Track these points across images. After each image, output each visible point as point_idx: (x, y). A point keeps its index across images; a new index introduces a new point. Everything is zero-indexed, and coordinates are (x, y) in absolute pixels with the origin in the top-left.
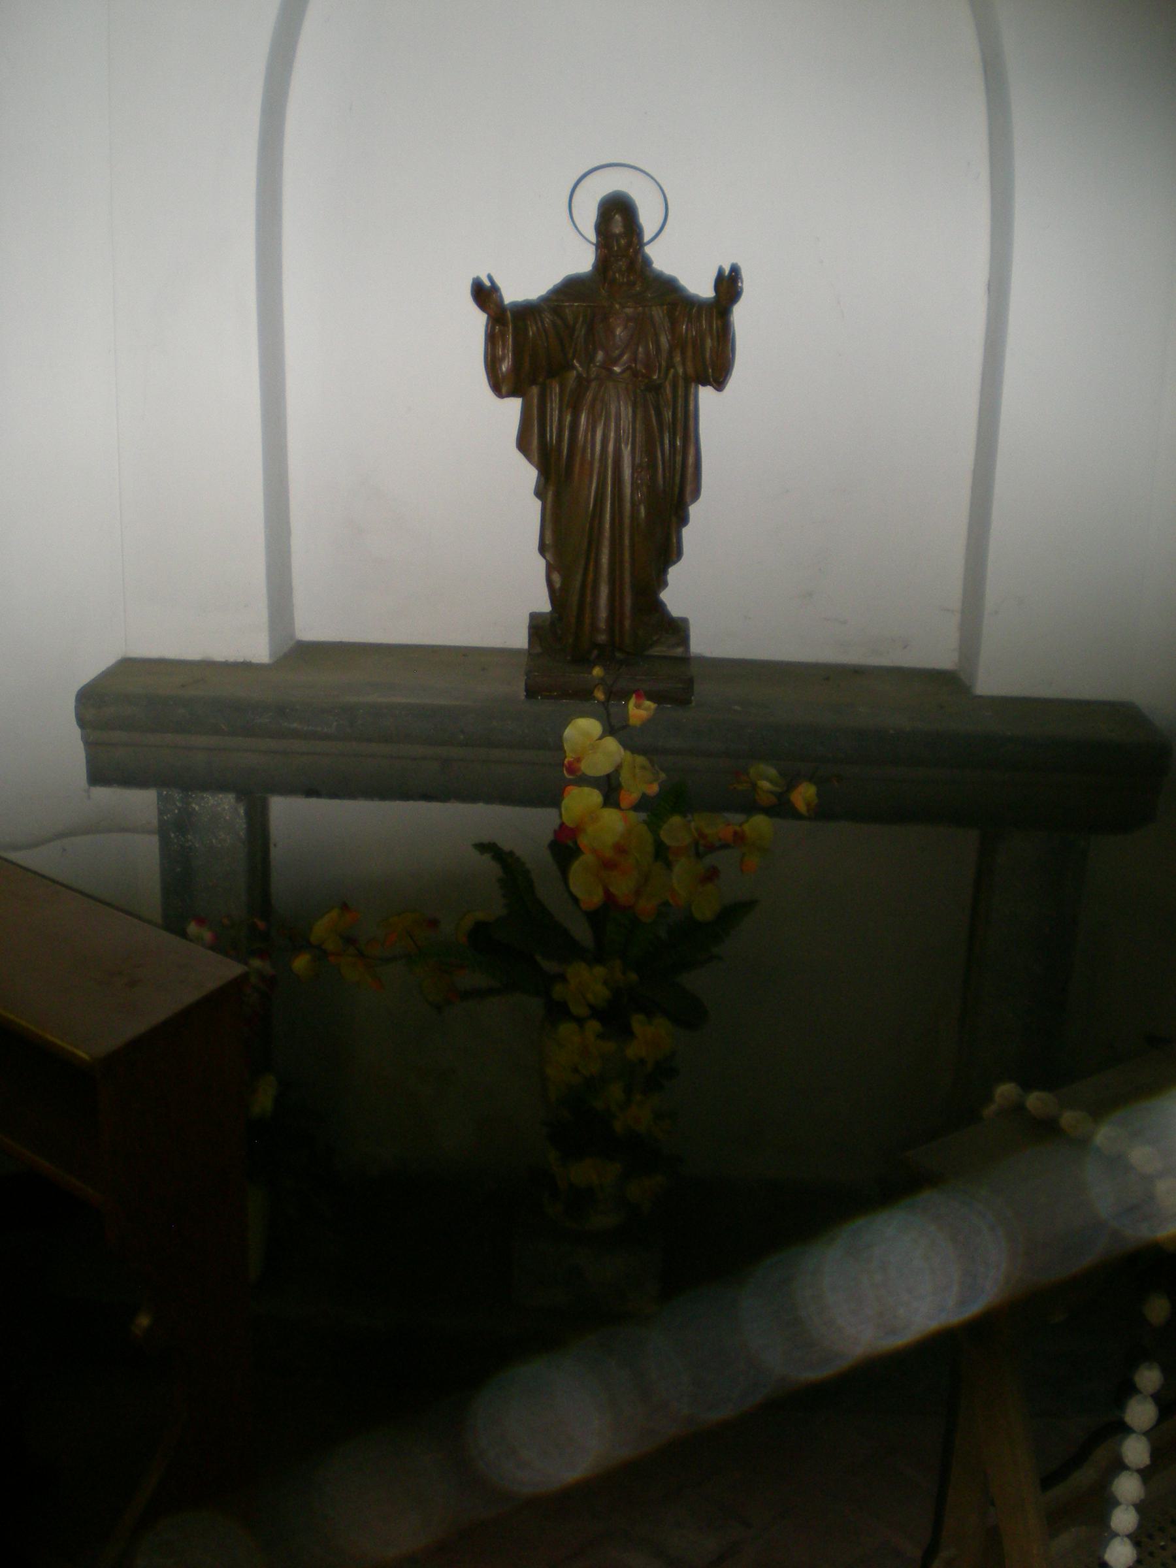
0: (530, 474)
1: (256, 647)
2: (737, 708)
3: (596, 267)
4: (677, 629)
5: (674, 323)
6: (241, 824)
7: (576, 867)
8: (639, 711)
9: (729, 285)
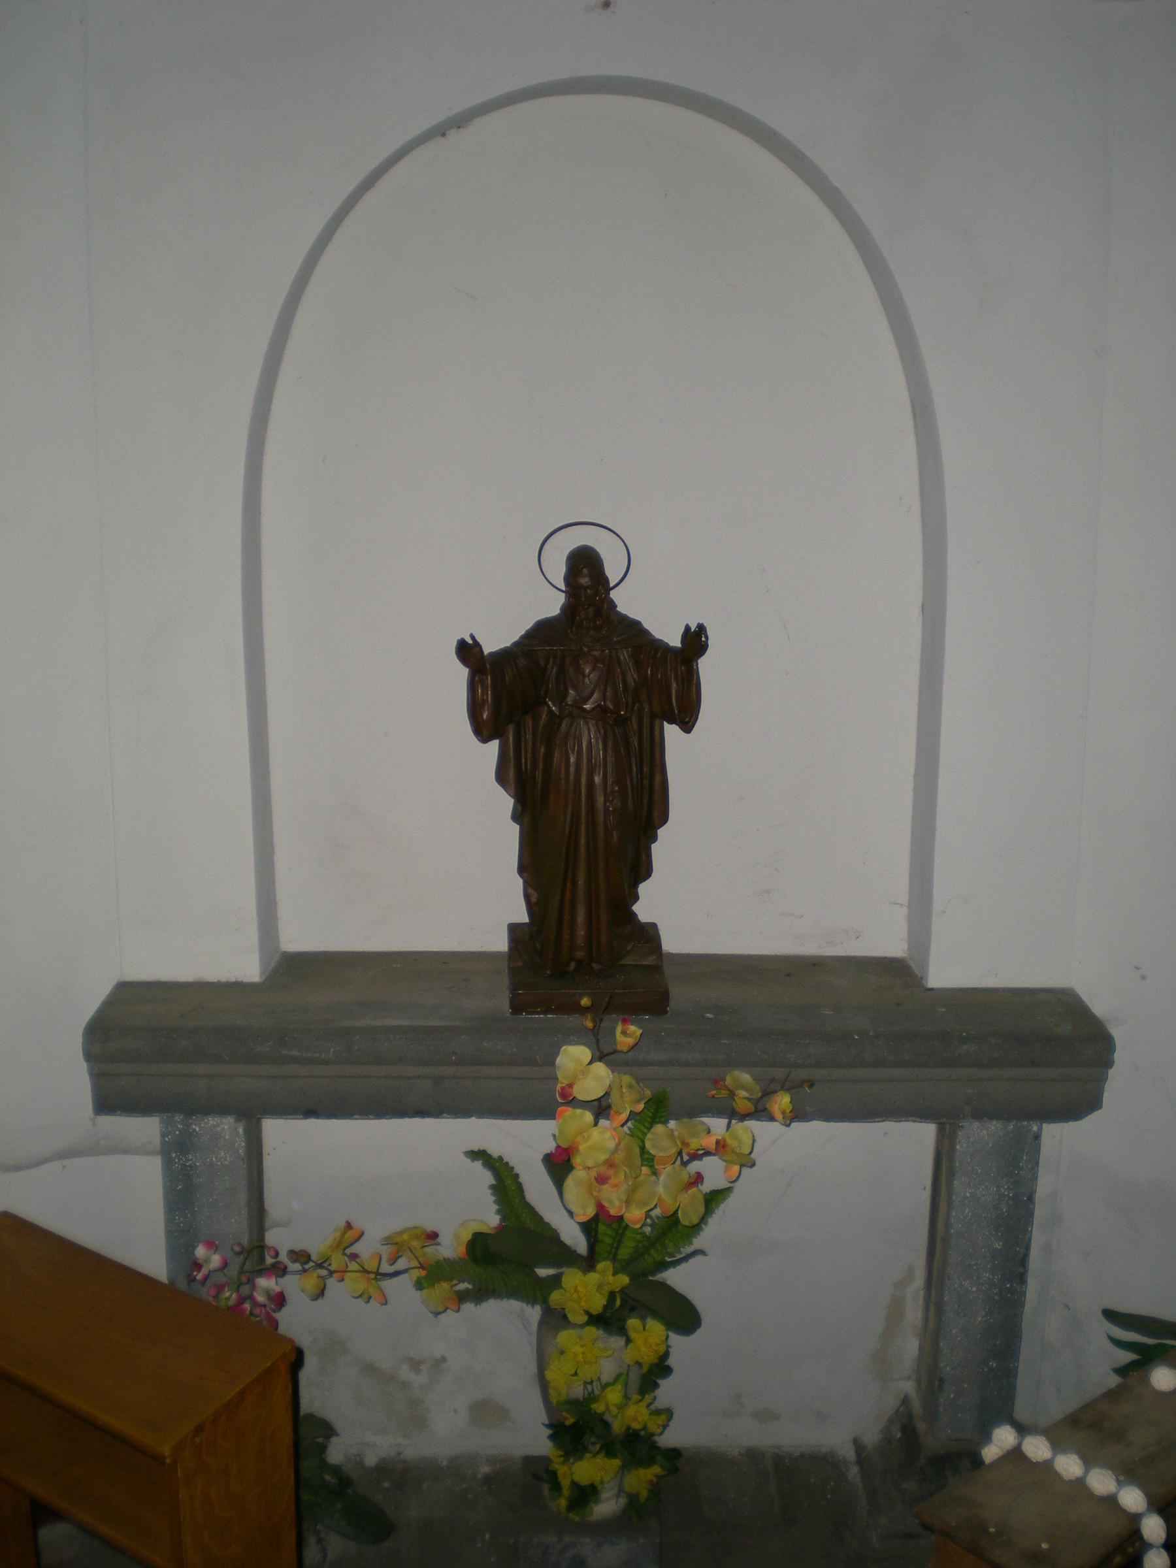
0: (506, 803)
1: (247, 967)
2: (709, 1015)
3: (564, 609)
4: (649, 935)
5: (638, 664)
6: (241, 1143)
7: (570, 1183)
8: (627, 1034)
9: (696, 641)
